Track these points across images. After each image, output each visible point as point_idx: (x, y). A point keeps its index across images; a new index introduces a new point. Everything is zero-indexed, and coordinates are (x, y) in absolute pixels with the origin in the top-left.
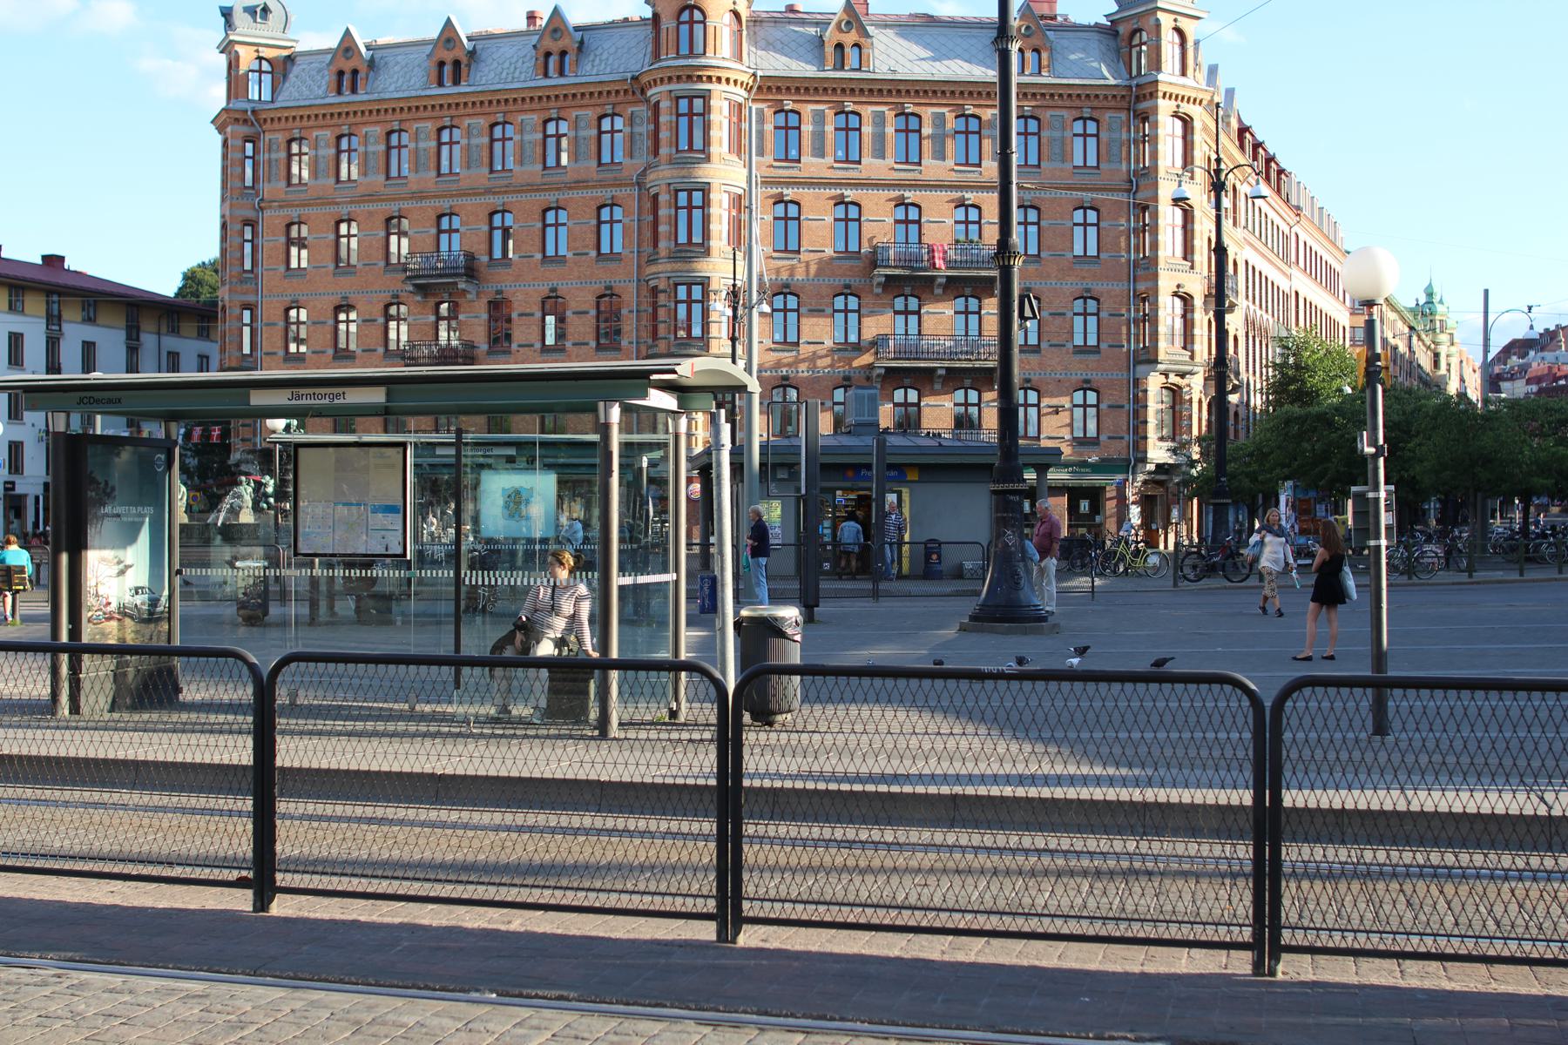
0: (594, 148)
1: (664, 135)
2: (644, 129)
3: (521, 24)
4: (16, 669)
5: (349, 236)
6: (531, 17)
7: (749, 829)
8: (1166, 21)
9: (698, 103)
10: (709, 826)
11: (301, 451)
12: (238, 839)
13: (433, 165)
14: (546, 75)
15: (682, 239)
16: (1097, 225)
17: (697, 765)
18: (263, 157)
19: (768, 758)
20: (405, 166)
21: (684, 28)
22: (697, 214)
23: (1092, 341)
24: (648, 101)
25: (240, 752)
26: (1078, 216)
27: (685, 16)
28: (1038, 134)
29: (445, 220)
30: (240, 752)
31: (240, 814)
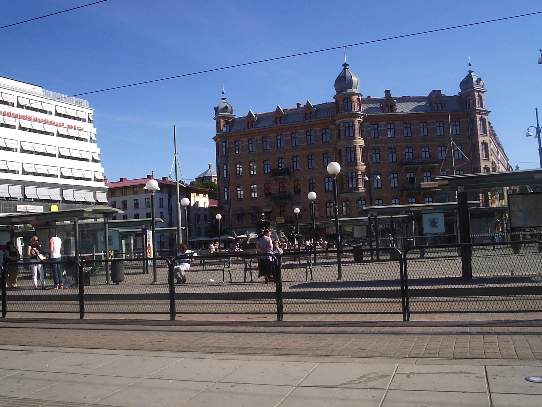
0: (321, 138)
1: (342, 133)
2: (335, 132)
4: (516, 257)
5: (239, 168)
6: (298, 104)
8: (476, 94)
9: (351, 124)
11: (103, 232)
12: (167, 308)
13: (276, 145)
14: (277, 124)
15: (349, 161)
16: (428, 151)
17: (76, 291)
18: (228, 146)
19: (87, 290)
20: (297, 142)
21: (346, 104)
22: (352, 153)
23: (380, 186)
24: (336, 124)
25: (167, 291)
26: (439, 149)
27: (346, 100)
28: (443, 126)
29: (280, 160)
30: (167, 291)
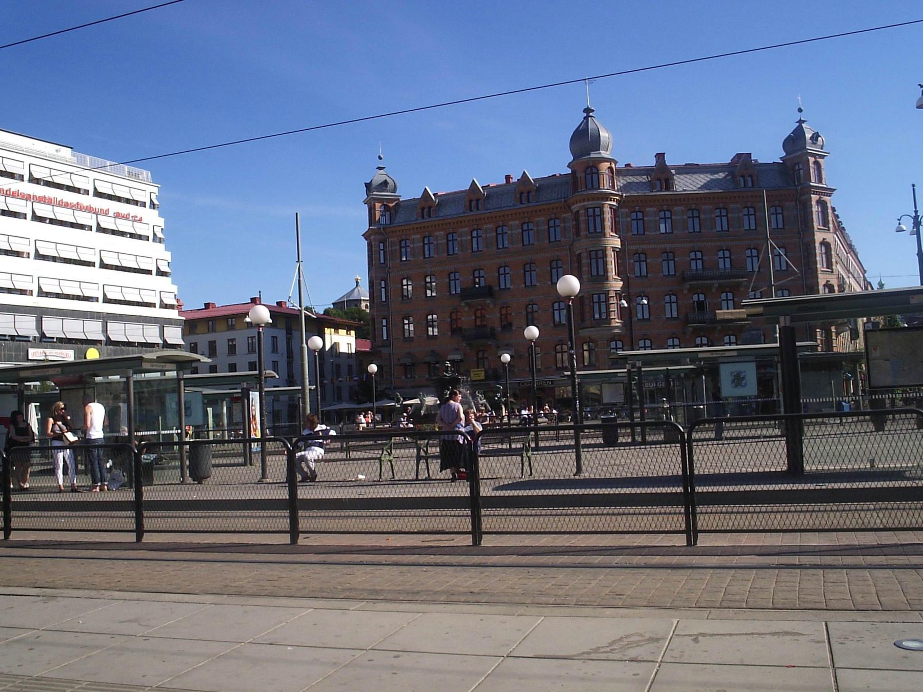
0: (547, 234)
1: (583, 226)
2: (571, 224)
3: (651, 162)
4: (878, 437)
5: (407, 285)
6: (508, 178)
7: (698, 510)
8: (811, 159)
9: (597, 210)
10: (287, 513)
11: (176, 395)
12: (285, 524)
13: (470, 247)
14: (471, 211)
15: (594, 273)
16: (730, 257)
17: (129, 495)
18: (388, 249)
19: (149, 494)
20: (506, 242)
21: (589, 177)
22: (600, 261)
23: (646, 316)
24: (572, 211)
25: (284, 494)
26: (748, 253)
27: (589, 171)
28: (754, 214)
29: (477, 272)
30: (284, 494)
31: (680, 513)
